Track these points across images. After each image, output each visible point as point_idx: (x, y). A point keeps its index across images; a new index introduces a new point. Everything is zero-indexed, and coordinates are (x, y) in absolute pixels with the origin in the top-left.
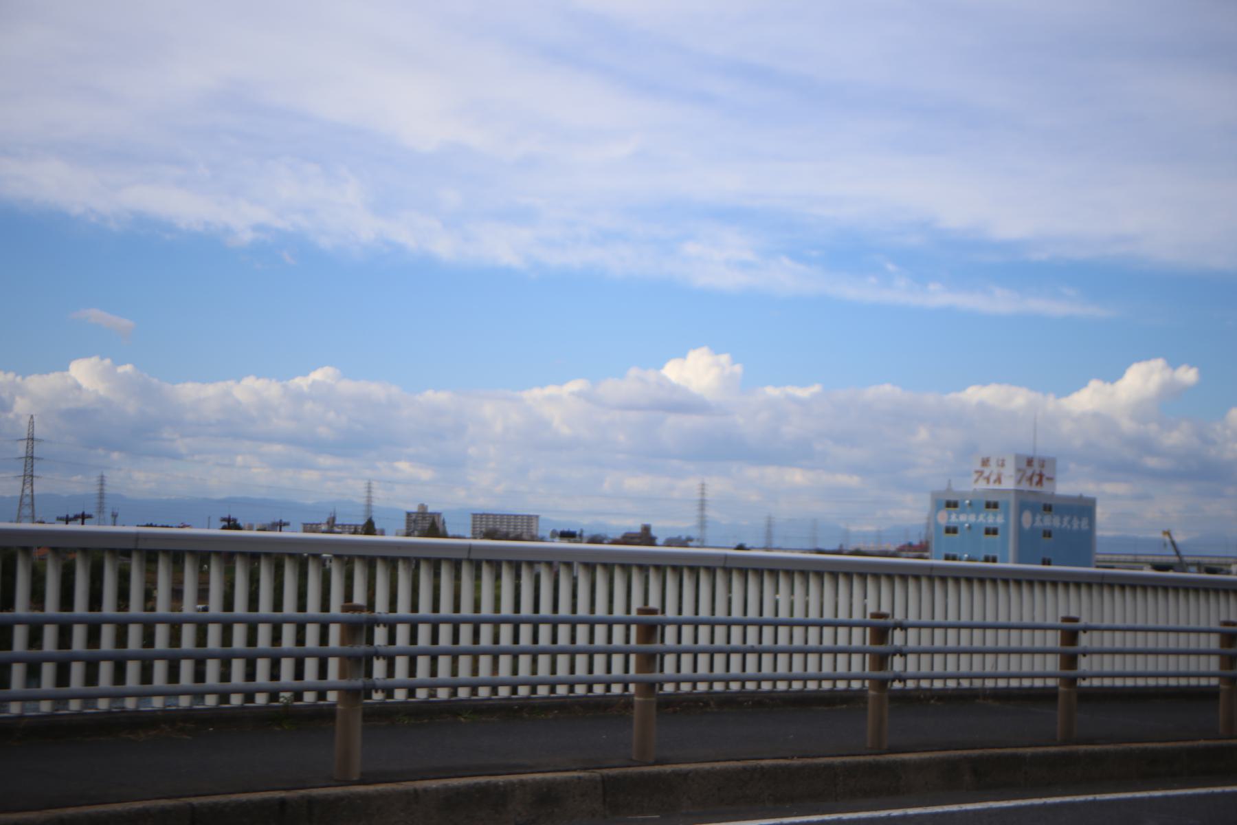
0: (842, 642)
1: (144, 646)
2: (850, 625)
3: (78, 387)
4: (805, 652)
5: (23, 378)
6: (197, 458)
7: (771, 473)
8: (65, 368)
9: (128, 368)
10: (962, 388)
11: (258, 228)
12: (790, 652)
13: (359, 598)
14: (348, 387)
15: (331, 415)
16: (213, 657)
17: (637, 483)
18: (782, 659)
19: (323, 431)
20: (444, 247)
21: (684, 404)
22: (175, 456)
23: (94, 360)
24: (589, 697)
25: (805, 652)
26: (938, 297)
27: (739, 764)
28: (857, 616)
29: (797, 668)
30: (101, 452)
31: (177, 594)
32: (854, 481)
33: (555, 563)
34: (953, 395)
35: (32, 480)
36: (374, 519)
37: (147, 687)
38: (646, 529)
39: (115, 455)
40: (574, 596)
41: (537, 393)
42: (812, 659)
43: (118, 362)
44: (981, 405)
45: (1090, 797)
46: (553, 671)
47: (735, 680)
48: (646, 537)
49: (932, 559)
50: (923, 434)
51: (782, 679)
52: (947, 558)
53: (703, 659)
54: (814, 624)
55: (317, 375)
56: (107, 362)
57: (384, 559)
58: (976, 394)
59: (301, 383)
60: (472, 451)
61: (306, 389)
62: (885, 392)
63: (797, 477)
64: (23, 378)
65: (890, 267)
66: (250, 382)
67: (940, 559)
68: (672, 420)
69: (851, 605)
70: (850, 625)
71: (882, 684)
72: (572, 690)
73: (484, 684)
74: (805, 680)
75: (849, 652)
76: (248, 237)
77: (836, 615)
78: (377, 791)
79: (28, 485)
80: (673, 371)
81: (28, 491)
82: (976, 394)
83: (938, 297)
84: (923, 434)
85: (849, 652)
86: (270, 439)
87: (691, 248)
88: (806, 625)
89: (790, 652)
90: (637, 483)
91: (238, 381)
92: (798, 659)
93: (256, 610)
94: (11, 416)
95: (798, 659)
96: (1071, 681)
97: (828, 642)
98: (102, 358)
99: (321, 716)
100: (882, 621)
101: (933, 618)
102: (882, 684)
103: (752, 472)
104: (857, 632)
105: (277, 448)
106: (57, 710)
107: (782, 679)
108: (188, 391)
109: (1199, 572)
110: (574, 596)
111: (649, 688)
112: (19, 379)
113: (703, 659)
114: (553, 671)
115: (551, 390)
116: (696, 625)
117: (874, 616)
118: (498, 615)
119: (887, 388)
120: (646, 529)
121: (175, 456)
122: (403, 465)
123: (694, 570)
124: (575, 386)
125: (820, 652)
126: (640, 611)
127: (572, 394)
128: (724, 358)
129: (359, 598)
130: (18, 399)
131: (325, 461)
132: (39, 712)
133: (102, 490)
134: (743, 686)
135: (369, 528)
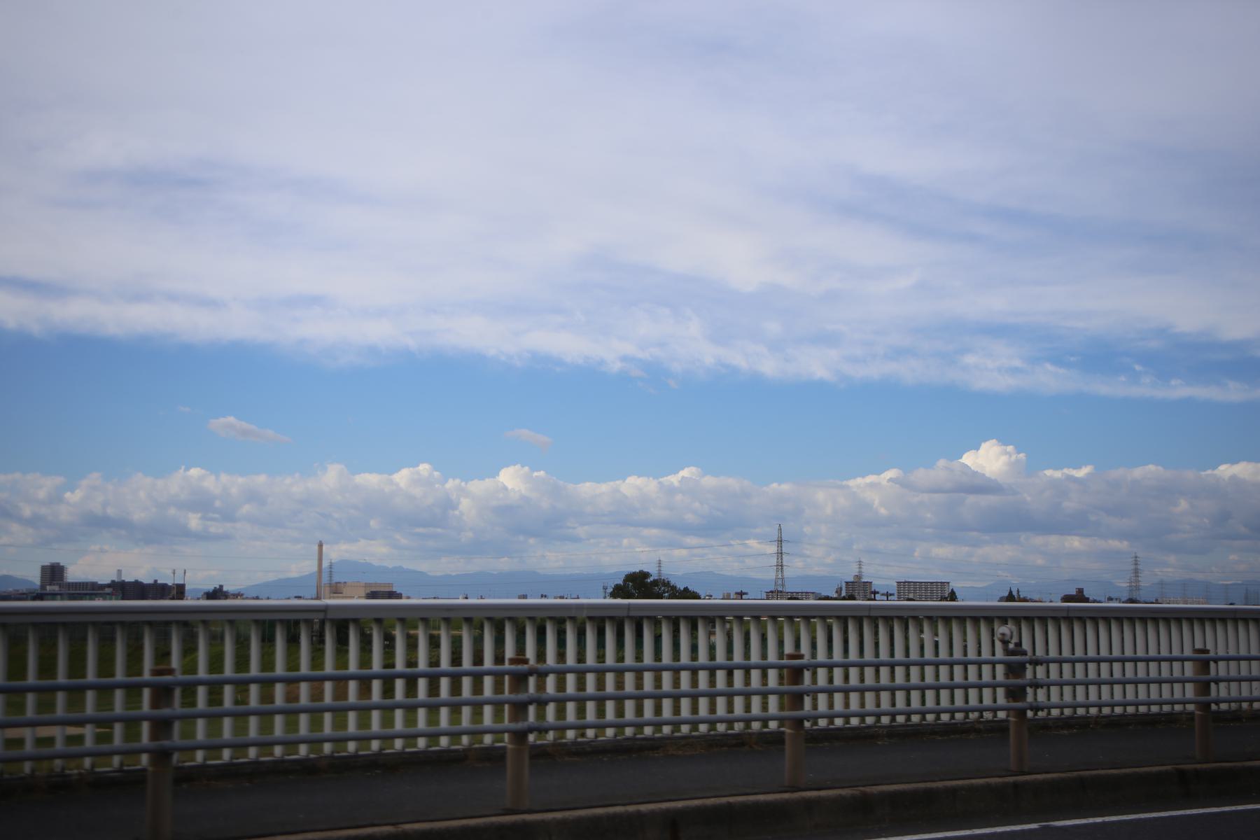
0: (1177, 673)
1: (693, 687)
2: (1182, 660)
3: (505, 488)
4: (1099, 684)
5: (466, 483)
6: (592, 541)
7: (1053, 541)
8: (495, 474)
9: (542, 473)
10: (1215, 467)
11: (624, 359)
12: (1074, 685)
13: (788, 648)
14: (709, 481)
15: (697, 505)
16: (571, 699)
17: (943, 551)
18: (1067, 690)
19: (689, 517)
20: (769, 367)
21: (981, 486)
22: (576, 540)
23: (518, 467)
24: (693, 737)
25: (1099, 684)
26: (1179, 390)
27: (1075, 774)
28: (1188, 652)
29: (1093, 697)
30: (521, 538)
31: (694, 649)
32: (1123, 545)
33: (713, 618)
34: (1209, 472)
35: (782, 569)
36: (955, 590)
37: (602, 721)
38: (1080, 591)
39: (532, 541)
40: (846, 642)
41: (859, 481)
42: (1105, 689)
43: (533, 469)
44: (1233, 478)
45: (1099, 820)
46: (908, 703)
47: (959, 711)
48: (1080, 596)
49: (413, 598)
50: (1183, 505)
51: (1119, 705)
52: (520, 597)
53: (930, 695)
54: (1117, 660)
55: (685, 473)
56: (526, 468)
57: (854, 617)
58: (1225, 471)
59: (674, 480)
60: (807, 530)
61: (676, 484)
62: (1148, 472)
63: (1075, 543)
64: (466, 483)
65: (1138, 368)
66: (633, 481)
67: (600, 598)
68: (971, 499)
69: (979, 644)
70: (1182, 660)
71: (1021, 713)
72: (863, 721)
73: (823, 717)
74: (1112, 706)
75: (1183, 681)
76: (617, 366)
77: (1123, 653)
78: (820, 797)
79: (780, 572)
80: (968, 459)
81: (780, 576)
82: (1225, 471)
83: (1179, 390)
84: (1183, 505)
85: (1183, 681)
86: (647, 524)
87: (970, 359)
88: (1135, 660)
89: (1074, 685)
90: (943, 551)
91: (624, 480)
92: (1105, 689)
93: (679, 660)
94: (457, 512)
95: (1067, 690)
96: (1021, 713)
97: (1117, 675)
98: (523, 467)
99: (493, 757)
100: (520, 667)
101: (1171, 652)
102: (1205, 706)
103: (1038, 540)
104: (1188, 665)
105: (654, 532)
106: (430, 747)
107: (1119, 705)
108: (587, 488)
109: (1120, 603)
110: (877, 644)
111: (1205, 706)
112: (463, 484)
113: (930, 695)
114: (923, 703)
115: (870, 479)
116: (965, 664)
117: (791, 657)
118: (966, 658)
119: (1151, 467)
120: (1080, 591)
121: (576, 540)
122: (752, 543)
123: (874, 621)
124: (891, 474)
125: (1123, 683)
126: (512, 661)
127: (891, 480)
128: (1010, 448)
129: (788, 648)
130: (462, 499)
131: (691, 540)
132: (605, 736)
133: (660, 570)
134: (953, 717)
135: (953, 596)
